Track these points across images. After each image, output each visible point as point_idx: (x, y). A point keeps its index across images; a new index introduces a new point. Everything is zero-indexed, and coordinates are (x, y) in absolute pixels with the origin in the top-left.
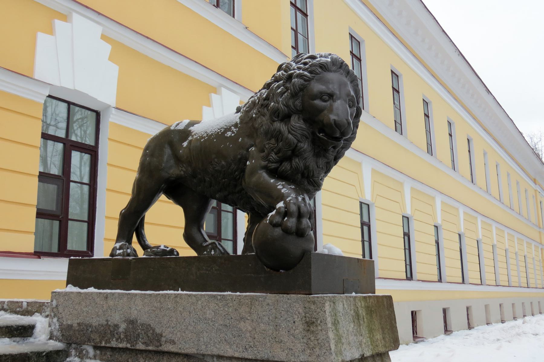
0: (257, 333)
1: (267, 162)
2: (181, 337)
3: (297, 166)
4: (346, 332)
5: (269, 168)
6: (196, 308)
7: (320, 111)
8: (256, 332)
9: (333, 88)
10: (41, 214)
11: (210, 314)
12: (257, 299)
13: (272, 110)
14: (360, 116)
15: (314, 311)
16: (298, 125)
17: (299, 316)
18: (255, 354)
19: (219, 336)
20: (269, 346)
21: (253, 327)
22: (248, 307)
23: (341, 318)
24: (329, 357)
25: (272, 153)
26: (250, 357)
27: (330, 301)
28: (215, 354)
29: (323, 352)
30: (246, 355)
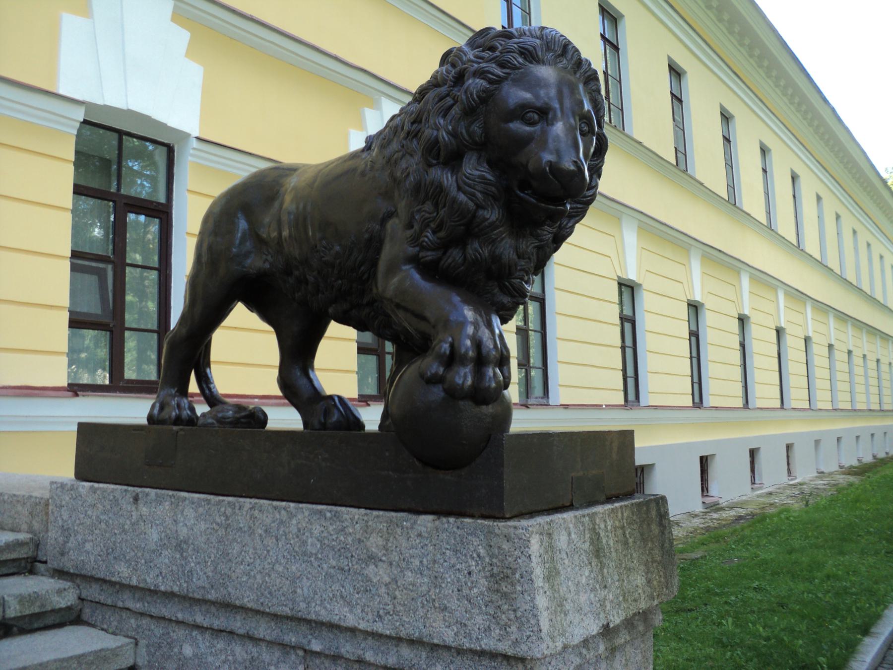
0: (400, 589)
1: (417, 249)
2: (262, 583)
3: (476, 256)
4: (573, 588)
5: (422, 260)
6: (289, 532)
7: (523, 142)
8: (398, 587)
9: (549, 95)
10: (77, 322)
11: (312, 545)
12: (399, 524)
13: (426, 143)
14: (605, 154)
15: (509, 554)
16: (477, 173)
17: (479, 562)
18: (396, 628)
19: (331, 587)
20: (422, 614)
21: (393, 577)
22: (381, 537)
23: (564, 563)
24: (537, 645)
25: (423, 235)
26: (388, 632)
27: (541, 534)
28: (324, 621)
29: (524, 634)
30: (380, 627)
